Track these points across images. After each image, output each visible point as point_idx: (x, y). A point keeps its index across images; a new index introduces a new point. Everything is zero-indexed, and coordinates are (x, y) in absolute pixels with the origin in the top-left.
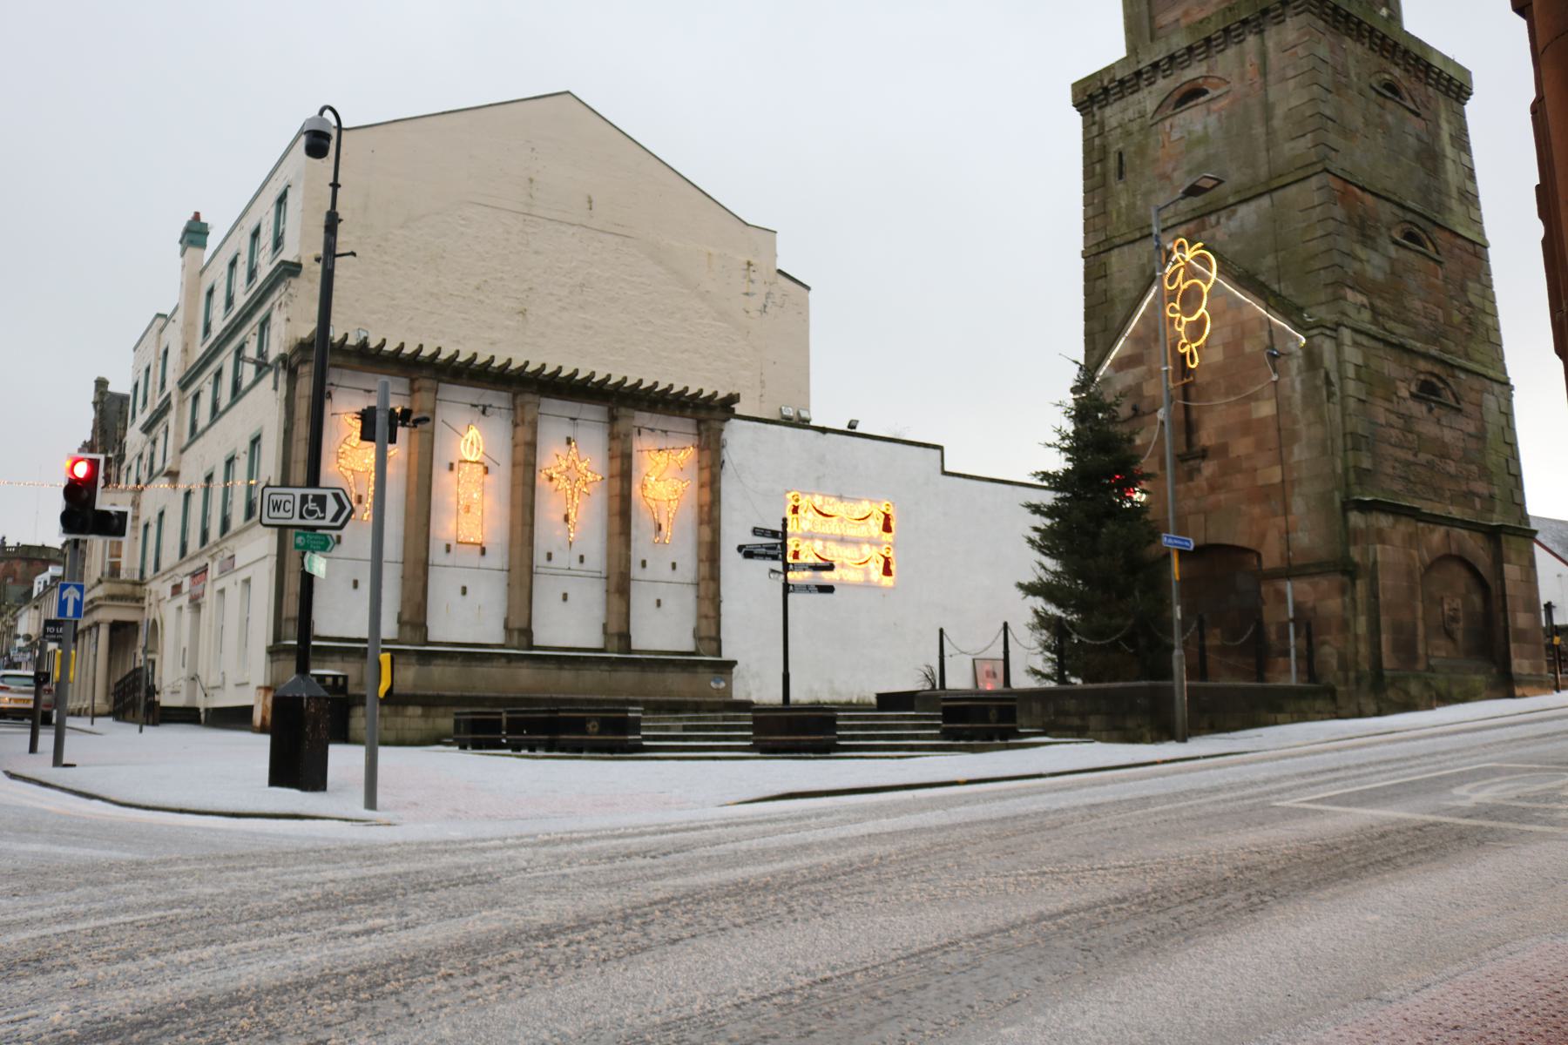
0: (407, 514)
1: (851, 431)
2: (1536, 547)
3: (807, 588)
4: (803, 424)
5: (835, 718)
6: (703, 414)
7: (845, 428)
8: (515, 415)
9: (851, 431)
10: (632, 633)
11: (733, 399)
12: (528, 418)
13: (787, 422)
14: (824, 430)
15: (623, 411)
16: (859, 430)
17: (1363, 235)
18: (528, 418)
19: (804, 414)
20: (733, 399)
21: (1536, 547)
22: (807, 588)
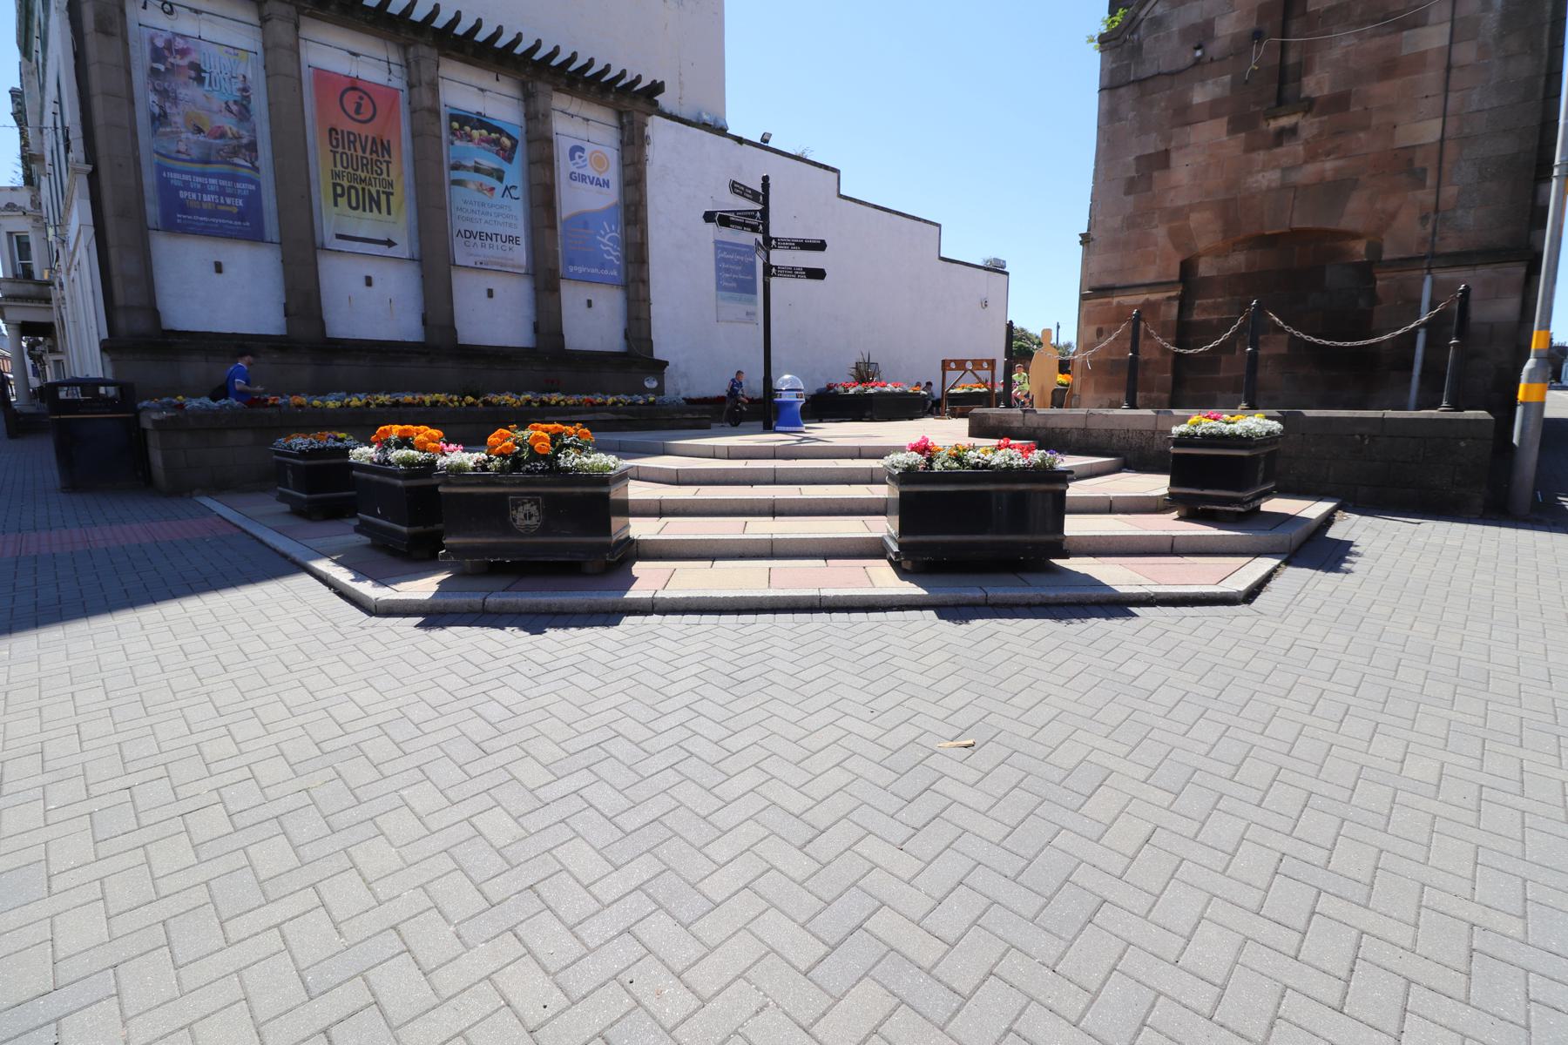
0: (77, 107)
1: (763, 145)
2: (1277, 562)
3: (793, 272)
4: (721, 131)
5: (1060, 507)
6: (626, 103)
7: (758, 141)
8: (409, 74)
9: (763, 145)
10: (457, 325)
11: (657, 88)
12: (425, 77)
13: (705, 126)
14: (740, 140)
15: (540, 86)
16: (770, 144)
17: (926, 448)
18: (425, 77)
19: (721, 123)
20: (657, 88)
21: (1277, 562)
22: (793, 272)
